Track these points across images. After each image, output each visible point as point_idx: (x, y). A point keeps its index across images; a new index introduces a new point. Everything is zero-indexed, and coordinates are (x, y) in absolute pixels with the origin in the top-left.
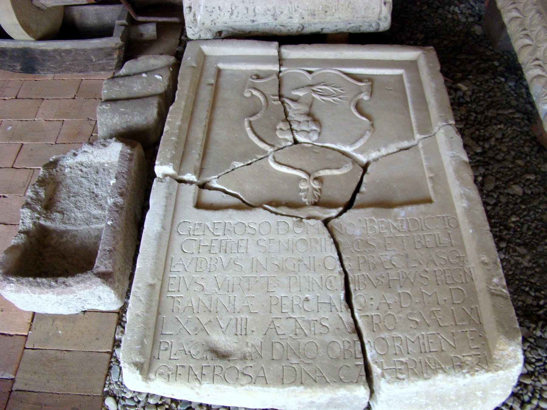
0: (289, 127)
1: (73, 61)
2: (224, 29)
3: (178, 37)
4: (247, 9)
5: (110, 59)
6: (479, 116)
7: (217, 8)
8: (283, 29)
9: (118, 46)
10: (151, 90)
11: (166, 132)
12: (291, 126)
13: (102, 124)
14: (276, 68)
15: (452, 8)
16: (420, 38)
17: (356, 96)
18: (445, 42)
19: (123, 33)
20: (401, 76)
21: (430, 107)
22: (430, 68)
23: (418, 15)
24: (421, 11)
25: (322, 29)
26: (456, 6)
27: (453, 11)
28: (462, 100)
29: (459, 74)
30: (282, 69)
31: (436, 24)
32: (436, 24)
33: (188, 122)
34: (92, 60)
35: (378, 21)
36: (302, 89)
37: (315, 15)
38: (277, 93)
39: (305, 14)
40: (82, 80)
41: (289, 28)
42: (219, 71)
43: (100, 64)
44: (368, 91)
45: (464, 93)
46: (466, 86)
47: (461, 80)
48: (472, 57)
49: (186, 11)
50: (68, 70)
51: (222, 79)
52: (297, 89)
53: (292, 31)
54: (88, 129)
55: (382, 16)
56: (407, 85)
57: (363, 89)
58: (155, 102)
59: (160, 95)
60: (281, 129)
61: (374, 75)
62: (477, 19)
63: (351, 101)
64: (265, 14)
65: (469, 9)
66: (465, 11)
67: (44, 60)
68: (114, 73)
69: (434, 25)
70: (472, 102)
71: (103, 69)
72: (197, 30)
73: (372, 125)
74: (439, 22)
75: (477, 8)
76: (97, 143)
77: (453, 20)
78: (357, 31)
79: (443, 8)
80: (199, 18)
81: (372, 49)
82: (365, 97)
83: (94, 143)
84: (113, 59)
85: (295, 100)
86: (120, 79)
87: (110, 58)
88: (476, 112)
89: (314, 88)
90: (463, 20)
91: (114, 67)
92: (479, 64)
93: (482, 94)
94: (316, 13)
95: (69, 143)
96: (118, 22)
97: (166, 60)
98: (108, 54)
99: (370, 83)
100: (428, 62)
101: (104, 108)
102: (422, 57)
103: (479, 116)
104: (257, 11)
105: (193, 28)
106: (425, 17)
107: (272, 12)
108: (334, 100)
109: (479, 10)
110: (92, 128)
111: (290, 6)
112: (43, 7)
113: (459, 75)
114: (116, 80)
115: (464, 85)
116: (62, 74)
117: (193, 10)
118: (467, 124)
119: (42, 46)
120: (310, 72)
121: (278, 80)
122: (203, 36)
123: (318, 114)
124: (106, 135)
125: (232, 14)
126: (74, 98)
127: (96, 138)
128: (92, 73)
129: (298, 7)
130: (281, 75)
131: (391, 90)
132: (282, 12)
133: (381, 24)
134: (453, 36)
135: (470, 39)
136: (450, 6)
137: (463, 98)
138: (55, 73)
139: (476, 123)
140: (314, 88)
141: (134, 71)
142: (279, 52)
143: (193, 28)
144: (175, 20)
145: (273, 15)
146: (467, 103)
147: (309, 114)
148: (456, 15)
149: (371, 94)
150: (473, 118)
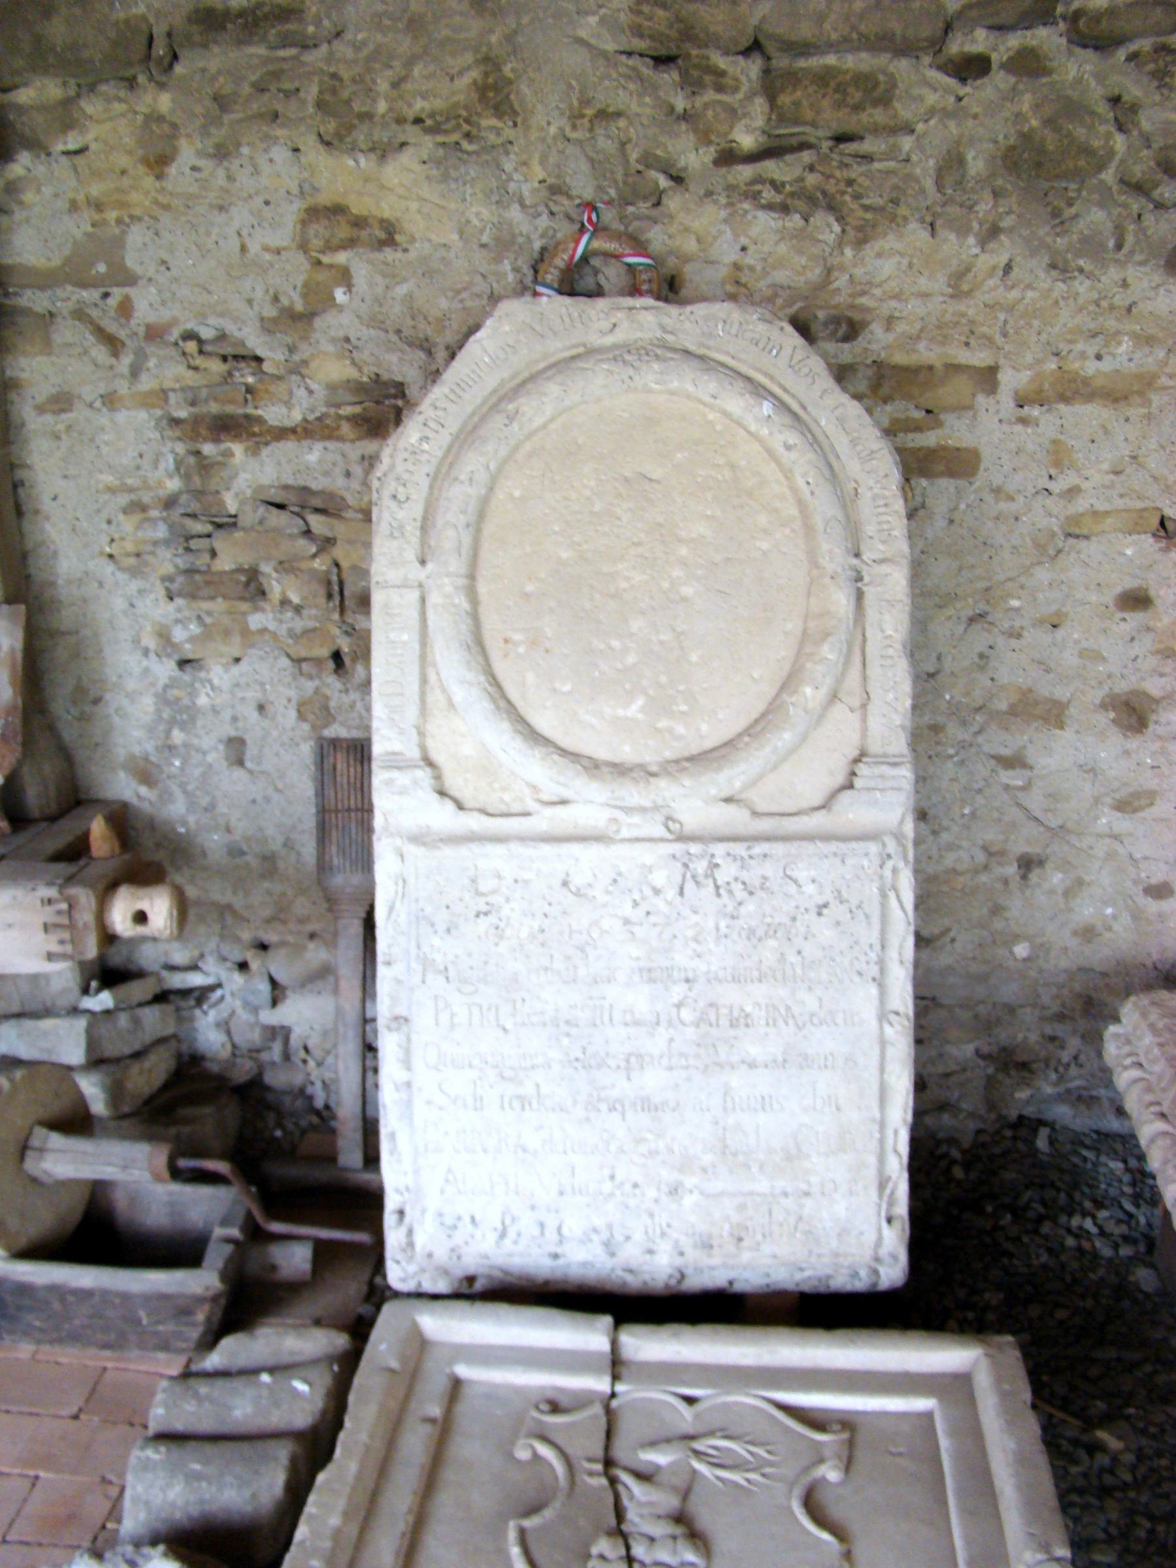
0: (623, 1552)
1: (91, 1317)
2: (481, 1271)
3: (365, 1276)
4: (542, 1225)
5: (187, 1324)
6: (1161, 1528)
7: (467, 1219)
8: (629, 1278)
9: (210, 1293)
10: (277, 1419)
11: (303, 1542)
12: (628, 1548)
13: (136, 1500)
14: (603, 1385)
15: (1075, 1221)
16: (994, 1302)
17: (807, 1469)
18: (1061, 1314)
19: (229, 1261)
20: (928, 1416)
21: (1003, 1506)
22: (1004, 1396)
23: (988, 1240)
24: (996, 1228)
25: (731, 1283)
26: (1085, 1214)
27: (1081, 1228)
28: (1108, 1480)
29: (1099, 1403)
30: (620, 1388)
31: (1035, 1262)
32: (1035, 1262)
33: (361, 1518)
34: (139, 1322)
35: (874, 1264)
36: (665, 1446)
37: (711, 1247)
38: (599, 1452)
39: (686, 1243)
40: (105, 1369)
41: (647, 1277)
42: (457, 1384)
43: (157, 1333)
44: (839, 1458)
45: (1115, 1459)
46: (1119, 1438)
47: (1106, 1420)
48: (1136, 1356)
49: (389, 1219)
50: (74, 1338)
51: (463, 1408)
52: (653, 1444)
53: (651, 1284)
54: (97, 1507)
55: (884, 1252)
56: (944, 1443)
57: (827, 1452)
58: (283, 1452)
59: (297, 1436)
60: (602, 1557)
61: (857, 1413)
62: (1142, 1248)
63: (792, 1484)
64: (585, 1240)
65: (1119, 1221)
66: (1111, 1227)
67: (19, 1308)
68: (190, 1361)
69: (1029, 1266)
70: (1137, 1485)
71: (165, 1347)
72: (412, 1268)
73: (848, 1555)
74: (1045, 1258)
75: (1142, 1220)
76: (115, 1554)
77: (1080, 1249)
78: (822, 1289)
79: (1055, 1221)
80: (420, 1240)
81: (852, 1341)
82: (831, 1474)
83: (108, 1555)
84: (194, 1325)
85: (643, 1476)
86: (202, 1380)
87: (185, 1319)
88: (1151, 1517)
89: (698, 1445)
90: (1107, 1252)
91: (192, 1345)
92: (1155, 1372)
93: (1164, 1462)
94: (715, 1243)
95: (40, 1545)
96: (219, 1232)
97: (324, 1341)
98: (182, 1309)
99: (845, 1435)
100: (998, 1380)
101: (148, 1458)
102: (984, 1364)
103: (1161, 1528)
104: (565, 1231)
105: (404, 1263)
106: (1009, 1246)
107: (605, 1235)
108: (748, 1480)
109: (1149, 1225)
110: (107, 1506)
111: (649, 1222)
112: (45, 1178)
113: (1100, 1405)
114: (192, 1382)
115: (1111, 1433)
116: (57, 1349)
117: (407, 1219)
118: (1127, 1550)
119: (23, 1273)
120: (690, 1400)
121: (603, 1421)
122: (428, 1286)
123: (705, 1519)
124: (142, 1530)
125: (503, 1235)
126: (76, 1417)
127: (113, 1541)
128: (135, 1353)
129: (669, 1226)
130: (614, 1403)
131: (900, 1454)
132: (628, 1238)
133: (882, 1270)
134: (1083, 1297)
135: (1126, 1304)
136: (1070, 1215)
137: (1112, 1472)
138: (39, 1342)
139: (1153, 1549)
140: (698, 1445)
141: (242, 1361)
142: (614, 1344)
143: (404, 1263)
144: (362, 1237)
145: (607, 1244)
146: (1125, 1486)
147: (680, 1518)
148: (1089, 1239)
149: (848, 1466)
150: (1142, 1534)
